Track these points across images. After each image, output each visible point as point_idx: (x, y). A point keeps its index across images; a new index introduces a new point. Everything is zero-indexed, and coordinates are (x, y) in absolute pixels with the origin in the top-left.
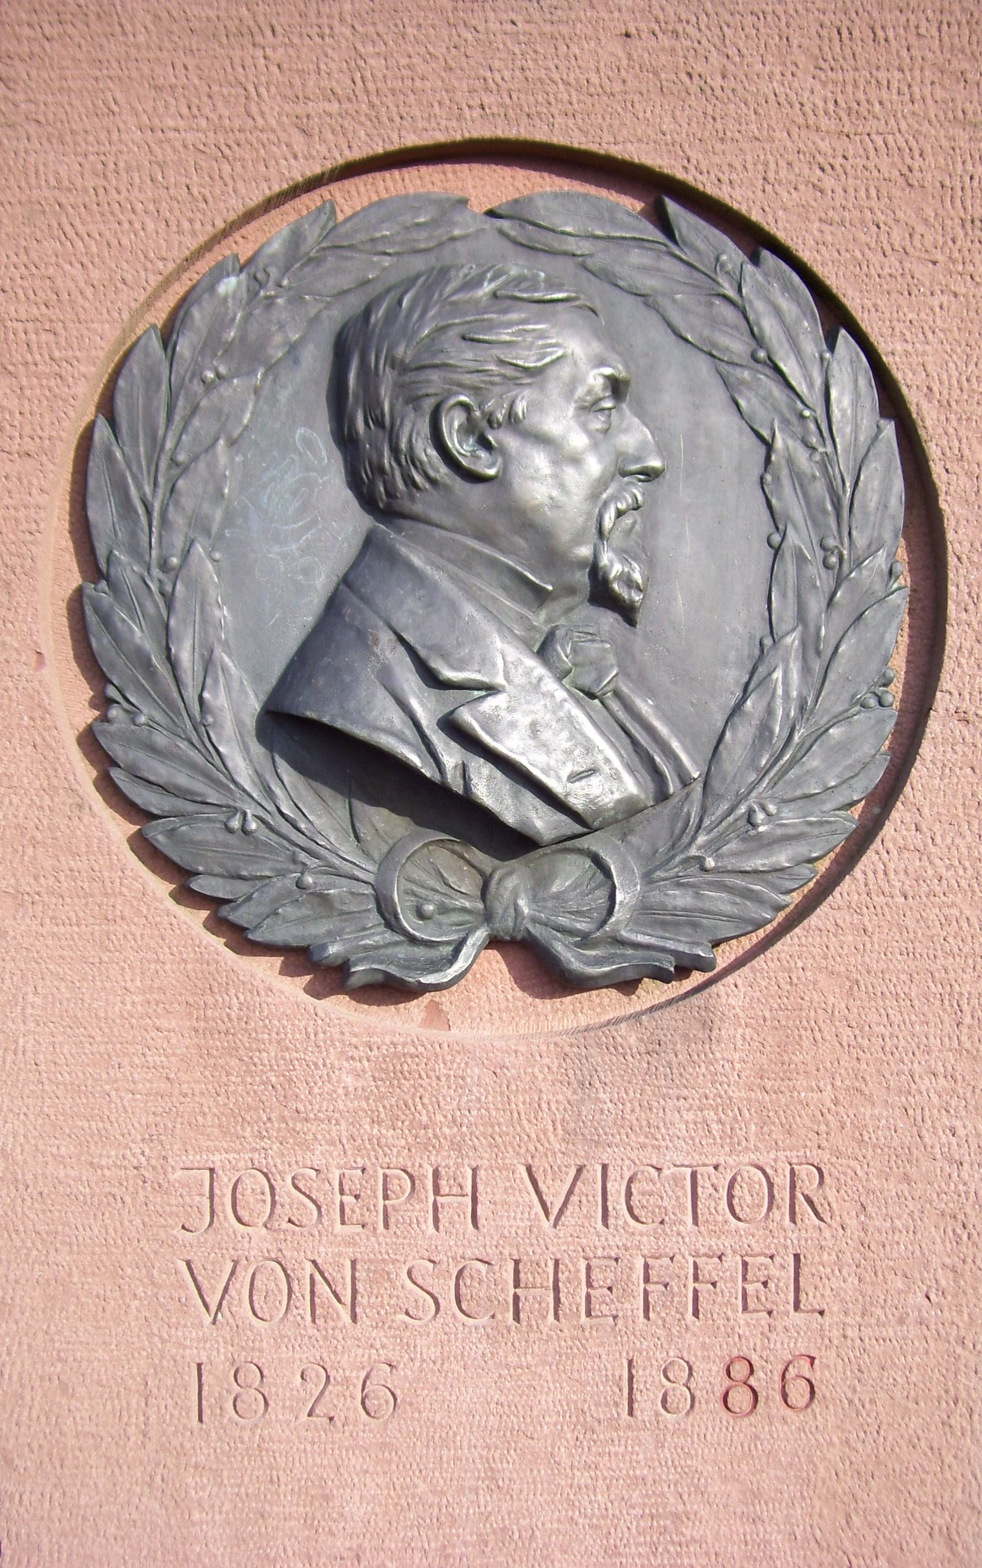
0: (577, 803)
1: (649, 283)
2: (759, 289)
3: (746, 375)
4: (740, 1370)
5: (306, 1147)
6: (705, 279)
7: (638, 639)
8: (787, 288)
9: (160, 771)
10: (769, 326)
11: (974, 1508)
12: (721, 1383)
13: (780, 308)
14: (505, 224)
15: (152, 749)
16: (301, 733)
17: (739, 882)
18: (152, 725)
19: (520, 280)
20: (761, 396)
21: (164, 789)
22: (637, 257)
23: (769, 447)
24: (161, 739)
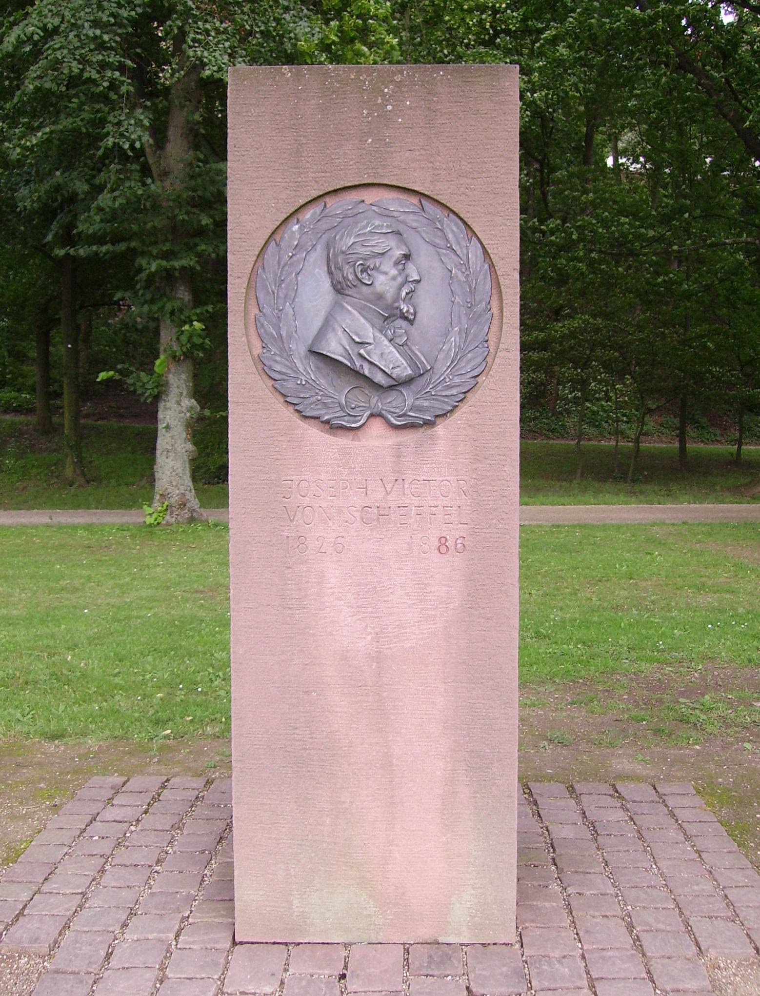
0: (394, 376)
1: (415, 225)
2: (448, 225)
3: (444, 251)
4: (443, 540)
5: (319, 473)
6: (431, 221)
7: (413, 330)
8: (456, 225)
9: (278, 368)
10: (450, 236)
11: (752, 940)
12: (437, 544)
13: (452, 229)
14: (374, 208)
15: (276, 361)
16: (313, 352)
17: (442, 399)
18: (275, 354)
19: (379, 226)
20: (450, 261)
21: (279, 372)
22: (411, 217)
23: (451, 272)
24: (278, 358)
